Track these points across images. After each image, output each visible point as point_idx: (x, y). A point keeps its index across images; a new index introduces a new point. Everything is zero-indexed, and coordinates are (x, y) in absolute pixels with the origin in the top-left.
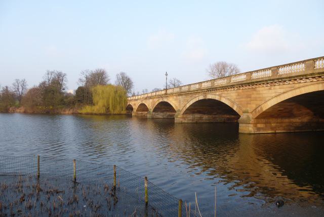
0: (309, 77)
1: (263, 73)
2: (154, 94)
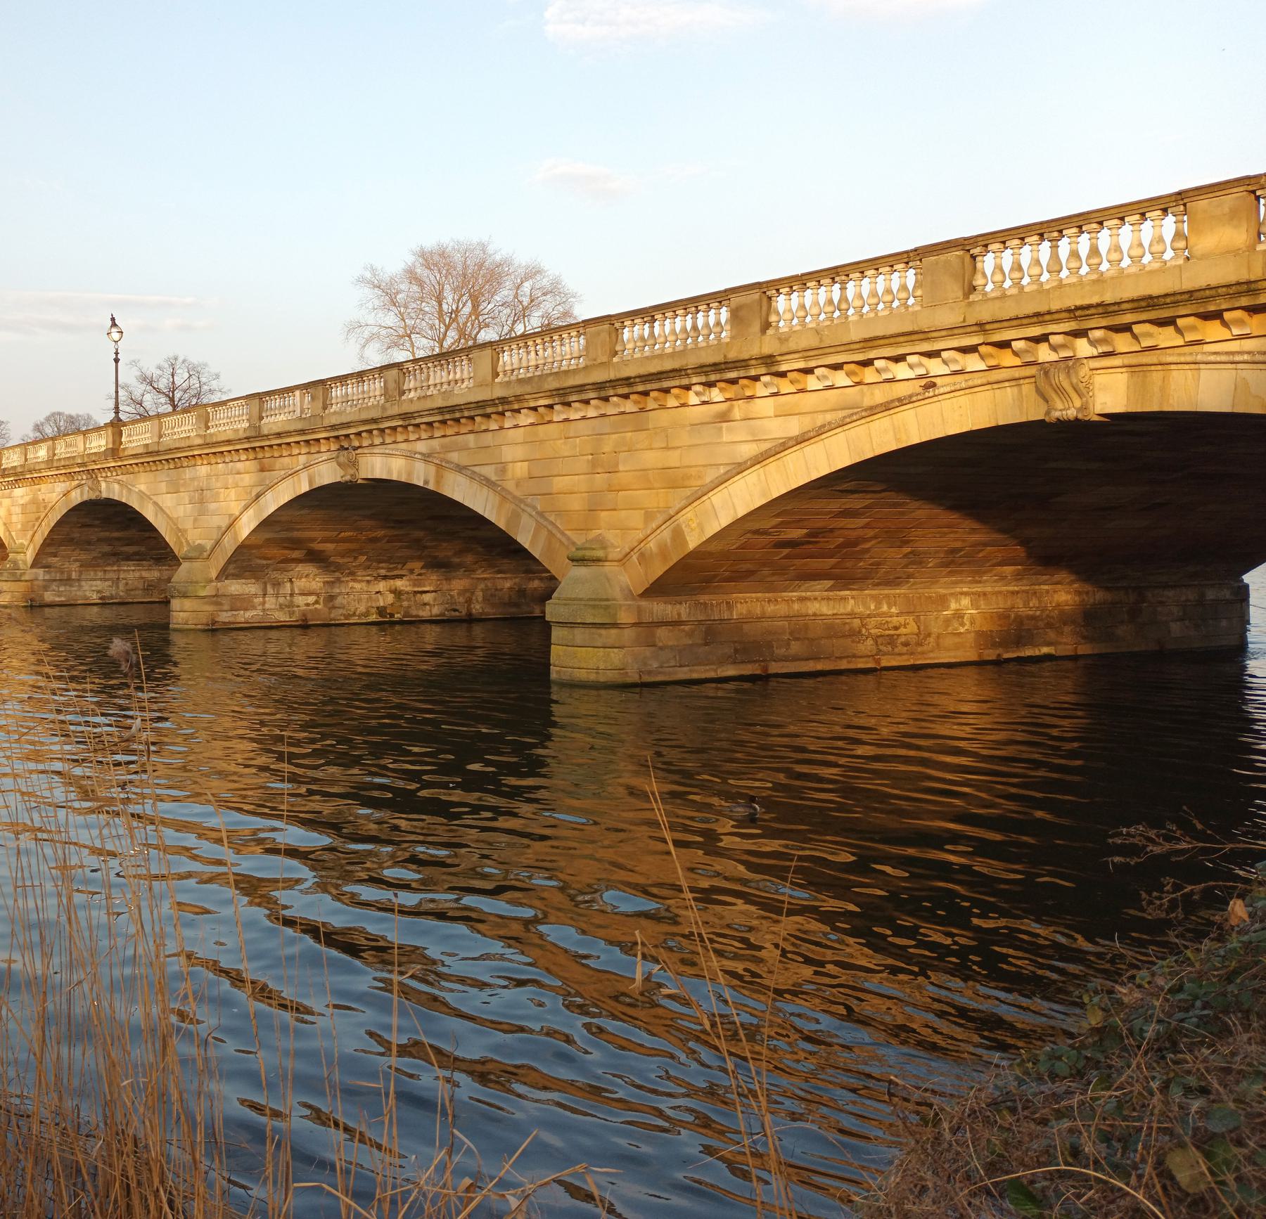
0: (1128, 318)
1: (681, 322)
2: (42, 453)
